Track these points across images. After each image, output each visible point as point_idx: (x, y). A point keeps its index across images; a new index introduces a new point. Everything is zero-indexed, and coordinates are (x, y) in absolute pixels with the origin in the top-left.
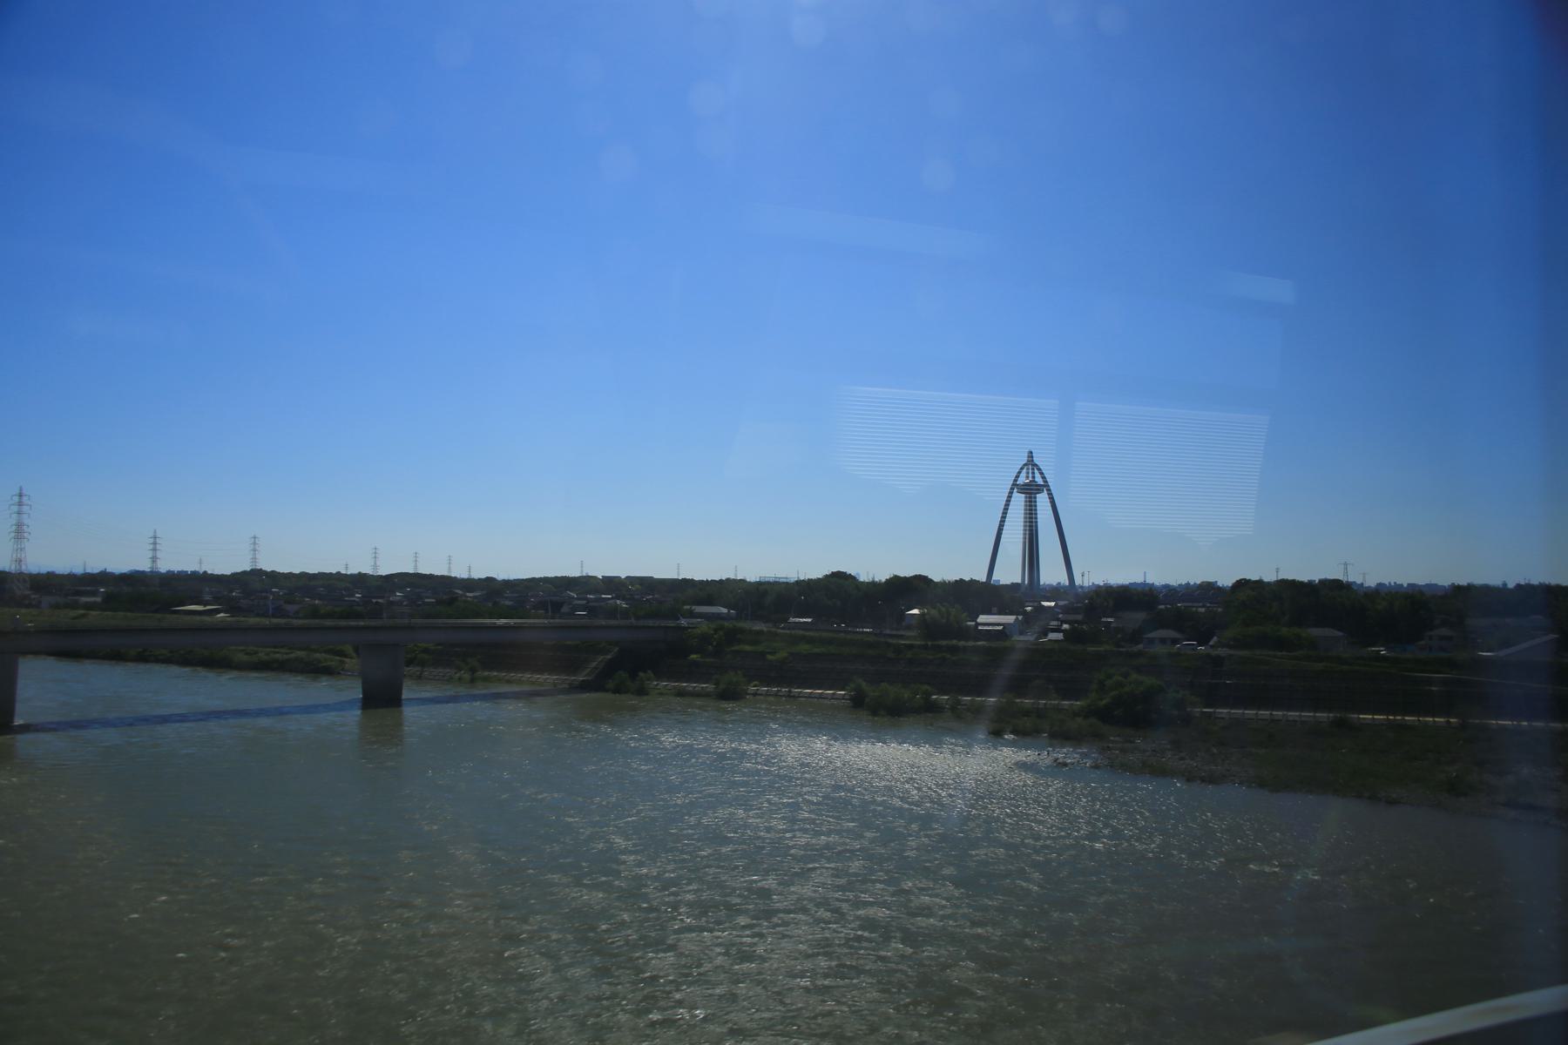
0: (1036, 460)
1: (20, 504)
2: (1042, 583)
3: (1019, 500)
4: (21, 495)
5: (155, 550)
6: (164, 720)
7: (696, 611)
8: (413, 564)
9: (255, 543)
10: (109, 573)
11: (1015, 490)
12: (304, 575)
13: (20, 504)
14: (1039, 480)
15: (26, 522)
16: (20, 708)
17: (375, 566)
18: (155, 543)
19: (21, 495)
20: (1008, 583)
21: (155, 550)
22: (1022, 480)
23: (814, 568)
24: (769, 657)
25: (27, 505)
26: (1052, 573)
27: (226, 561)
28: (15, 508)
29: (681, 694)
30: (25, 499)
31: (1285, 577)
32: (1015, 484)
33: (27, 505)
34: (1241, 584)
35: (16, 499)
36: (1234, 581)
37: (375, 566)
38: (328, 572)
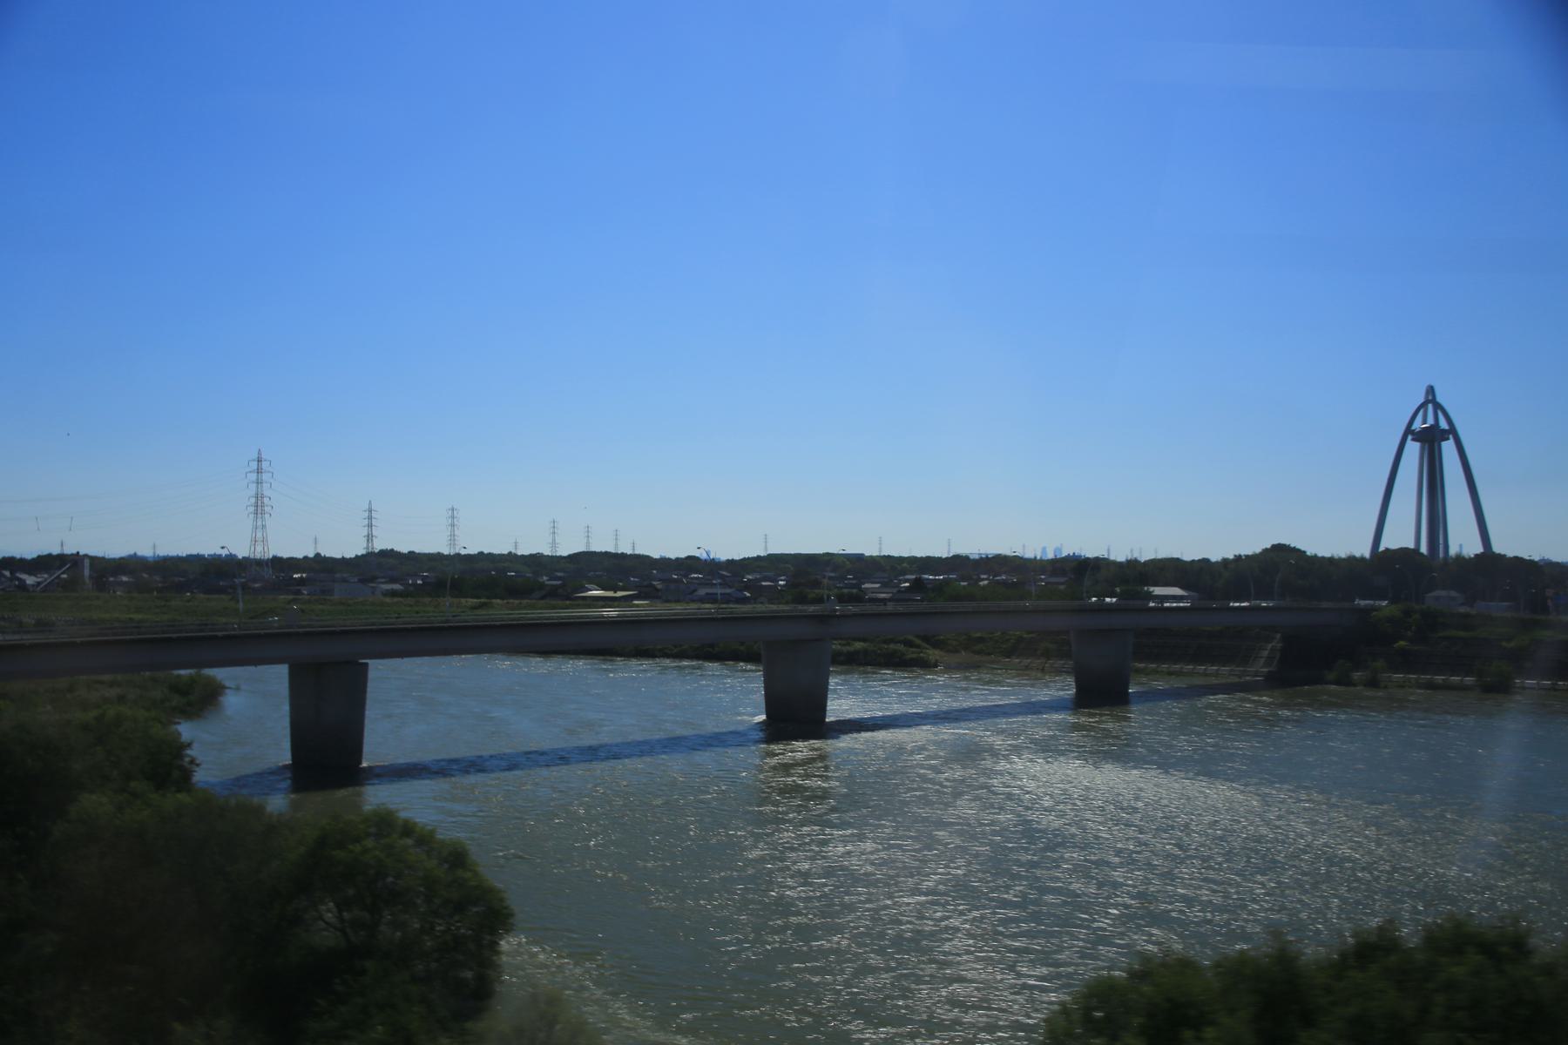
0: (1439, 399)
1: (259, 471)
2: (1453, 551)
3: (1413, 449)
4: (259, 461)
5: (370, 526)
6: (613, 753)
7: (1156, 593)
8: (764, 544)
9: (453, 517)
10: (329, 558)
11: (1410, 437)
12: (429, 554)
13: (259, 471)
14: (1443, 425)
15: (265, 493)
16: (366, 748)
17: (554, 544)
18: (370, 518)
19: (259, 461)
20: (1510, 553)
21: (370, 526)
22: (1418, 425)
23: (1251, 543)
24: (1504, 644)
25: (269, 472)
26: (1463, 540)
27: (345, 544)
28: (253, 477)
29: (1432, 686)
30: (265, 465)
31: (384, 548)
32: (1408, 431)
33: (269, 472)
34: (1516, 558)
35: (254, 465)
36: (195, 552)
37: (554, 544)
38: (683, 555)
